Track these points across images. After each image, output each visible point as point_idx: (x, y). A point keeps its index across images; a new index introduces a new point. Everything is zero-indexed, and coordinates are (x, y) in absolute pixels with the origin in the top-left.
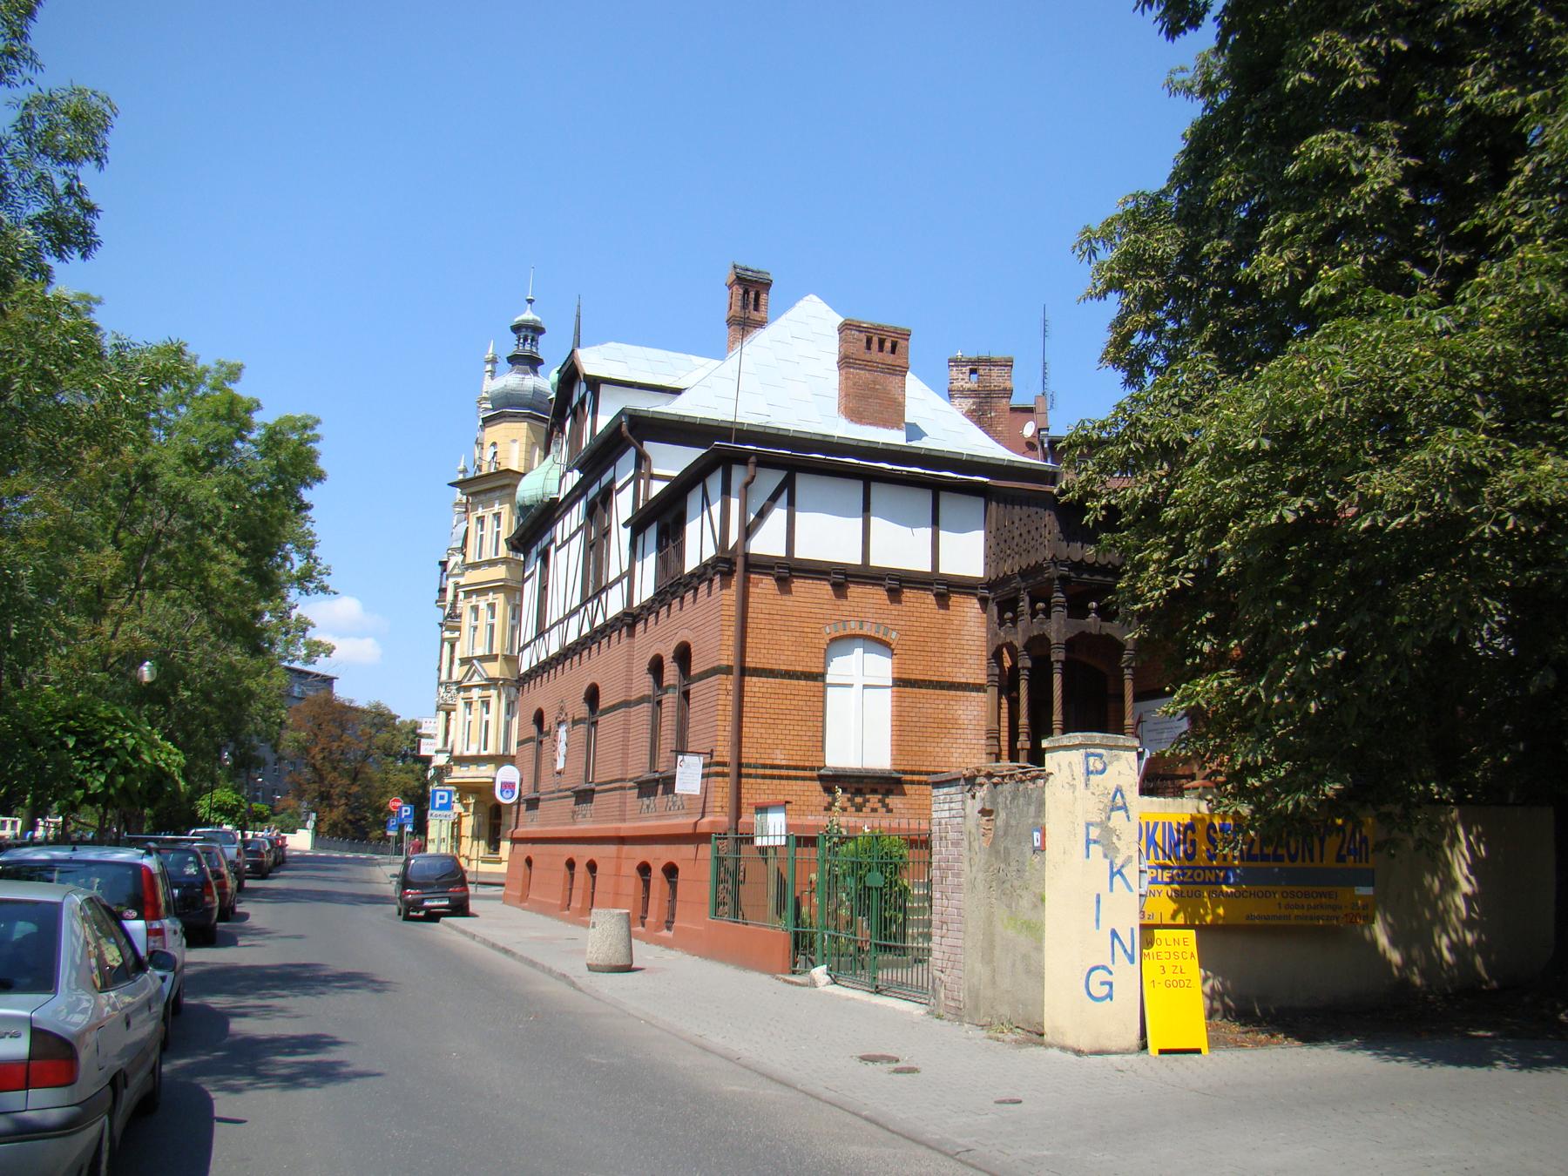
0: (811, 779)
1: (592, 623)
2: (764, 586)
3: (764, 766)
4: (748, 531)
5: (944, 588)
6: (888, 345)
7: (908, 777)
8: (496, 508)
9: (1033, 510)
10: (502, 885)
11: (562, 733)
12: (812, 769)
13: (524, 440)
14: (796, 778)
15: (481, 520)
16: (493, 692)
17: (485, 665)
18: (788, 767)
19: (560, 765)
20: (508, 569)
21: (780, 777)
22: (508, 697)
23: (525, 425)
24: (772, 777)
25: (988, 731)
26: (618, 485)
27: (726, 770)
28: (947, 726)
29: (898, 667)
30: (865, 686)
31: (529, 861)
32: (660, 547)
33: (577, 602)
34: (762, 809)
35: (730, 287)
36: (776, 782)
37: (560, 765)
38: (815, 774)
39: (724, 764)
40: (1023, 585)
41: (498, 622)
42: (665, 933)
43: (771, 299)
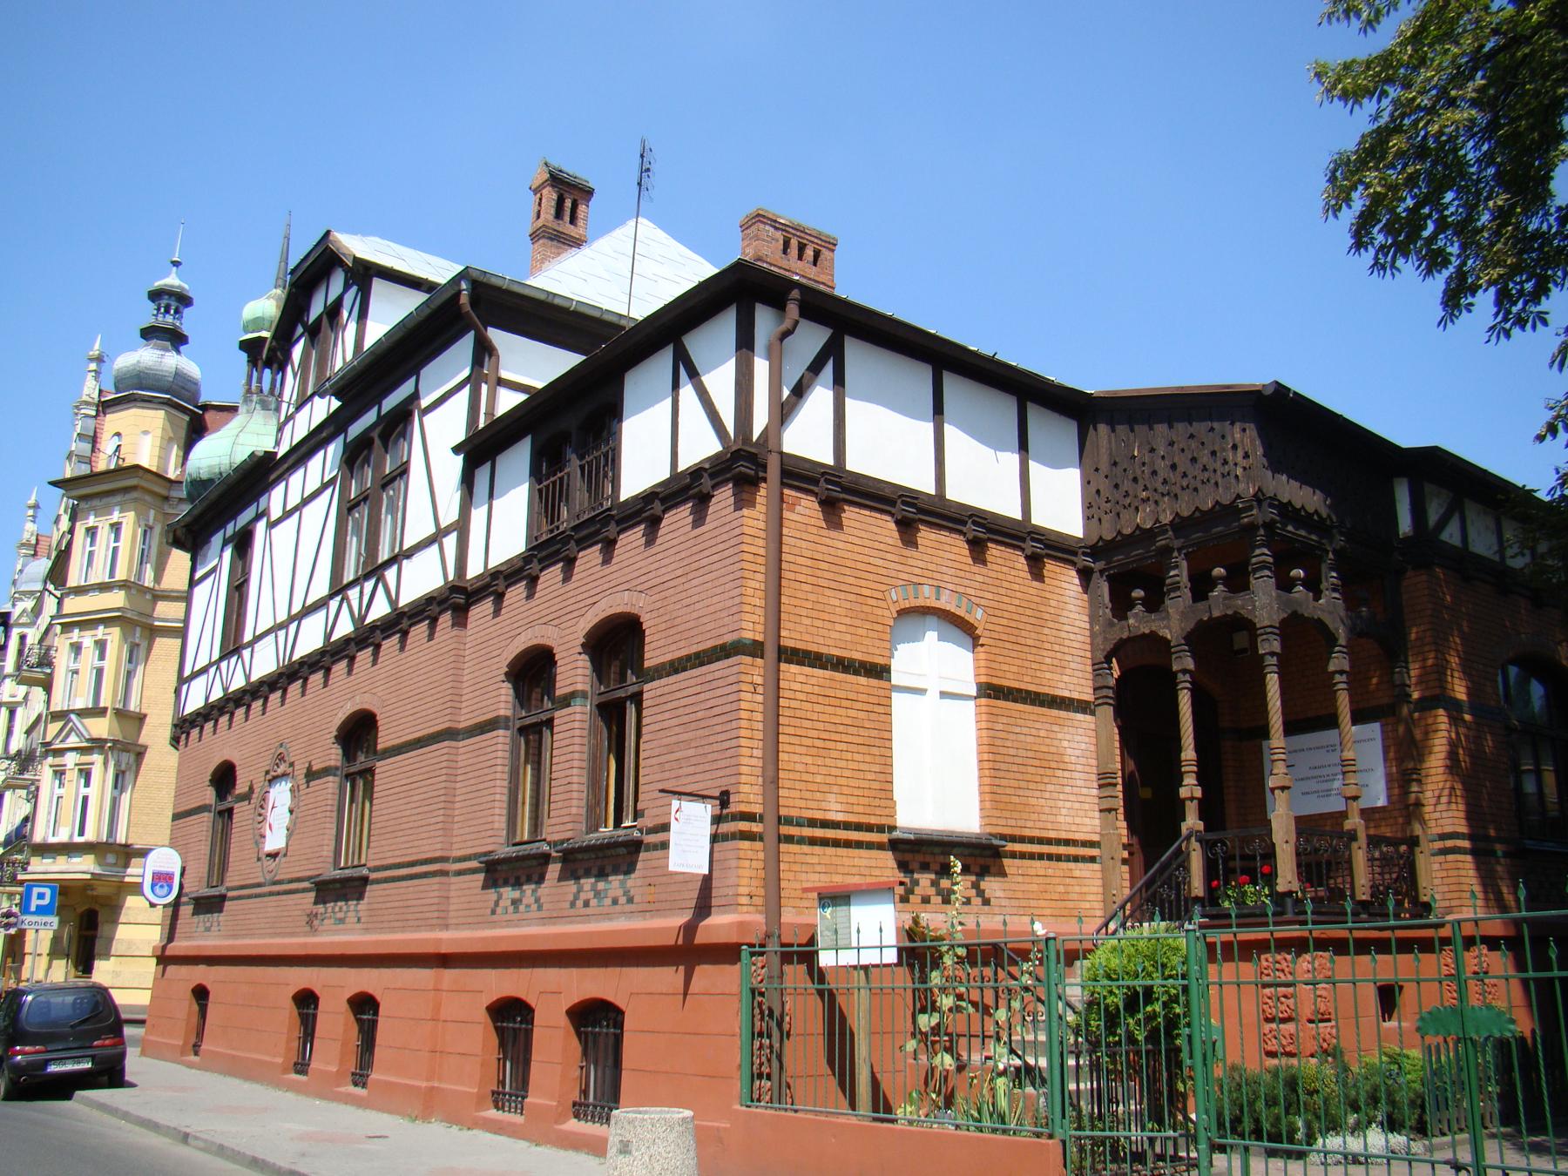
0: (880, 846)
1: (359, 620)
2: (804, 510)
3: (812, 823)
4: (783, 412)
6: (809, 253)
7: (1011, 847)
8: (116, 516)
9: (1200, 428)
10: (142, 1022)
11: (281, 795)
12: (880, 829)
13: (159, 432)
14: (859, 845)
15: (92, 532)
16: (97, 758)
17: (88, 721)
18: (847, 826)
19: (275, 840)
20: (128, 596)
21: (836, 843)
22: (118, 764)
23: (161, 414)
24: (824, 842)
25: (1102, 775)
26: (425, 403)
27: (756, 827)
28: (1049, 764)
30: (944, 695)
31: (201, 994)
32: (536, 474)
33: (321, 588)
34: (837, 897)
35: (537, 191)
36: (830, 850)
37: (275, 840)
38: (884, 838)
39: (750, 817)
40: (1177, 543)
41: (109, 665)
42: (193, 1058)
43: (591, 212)
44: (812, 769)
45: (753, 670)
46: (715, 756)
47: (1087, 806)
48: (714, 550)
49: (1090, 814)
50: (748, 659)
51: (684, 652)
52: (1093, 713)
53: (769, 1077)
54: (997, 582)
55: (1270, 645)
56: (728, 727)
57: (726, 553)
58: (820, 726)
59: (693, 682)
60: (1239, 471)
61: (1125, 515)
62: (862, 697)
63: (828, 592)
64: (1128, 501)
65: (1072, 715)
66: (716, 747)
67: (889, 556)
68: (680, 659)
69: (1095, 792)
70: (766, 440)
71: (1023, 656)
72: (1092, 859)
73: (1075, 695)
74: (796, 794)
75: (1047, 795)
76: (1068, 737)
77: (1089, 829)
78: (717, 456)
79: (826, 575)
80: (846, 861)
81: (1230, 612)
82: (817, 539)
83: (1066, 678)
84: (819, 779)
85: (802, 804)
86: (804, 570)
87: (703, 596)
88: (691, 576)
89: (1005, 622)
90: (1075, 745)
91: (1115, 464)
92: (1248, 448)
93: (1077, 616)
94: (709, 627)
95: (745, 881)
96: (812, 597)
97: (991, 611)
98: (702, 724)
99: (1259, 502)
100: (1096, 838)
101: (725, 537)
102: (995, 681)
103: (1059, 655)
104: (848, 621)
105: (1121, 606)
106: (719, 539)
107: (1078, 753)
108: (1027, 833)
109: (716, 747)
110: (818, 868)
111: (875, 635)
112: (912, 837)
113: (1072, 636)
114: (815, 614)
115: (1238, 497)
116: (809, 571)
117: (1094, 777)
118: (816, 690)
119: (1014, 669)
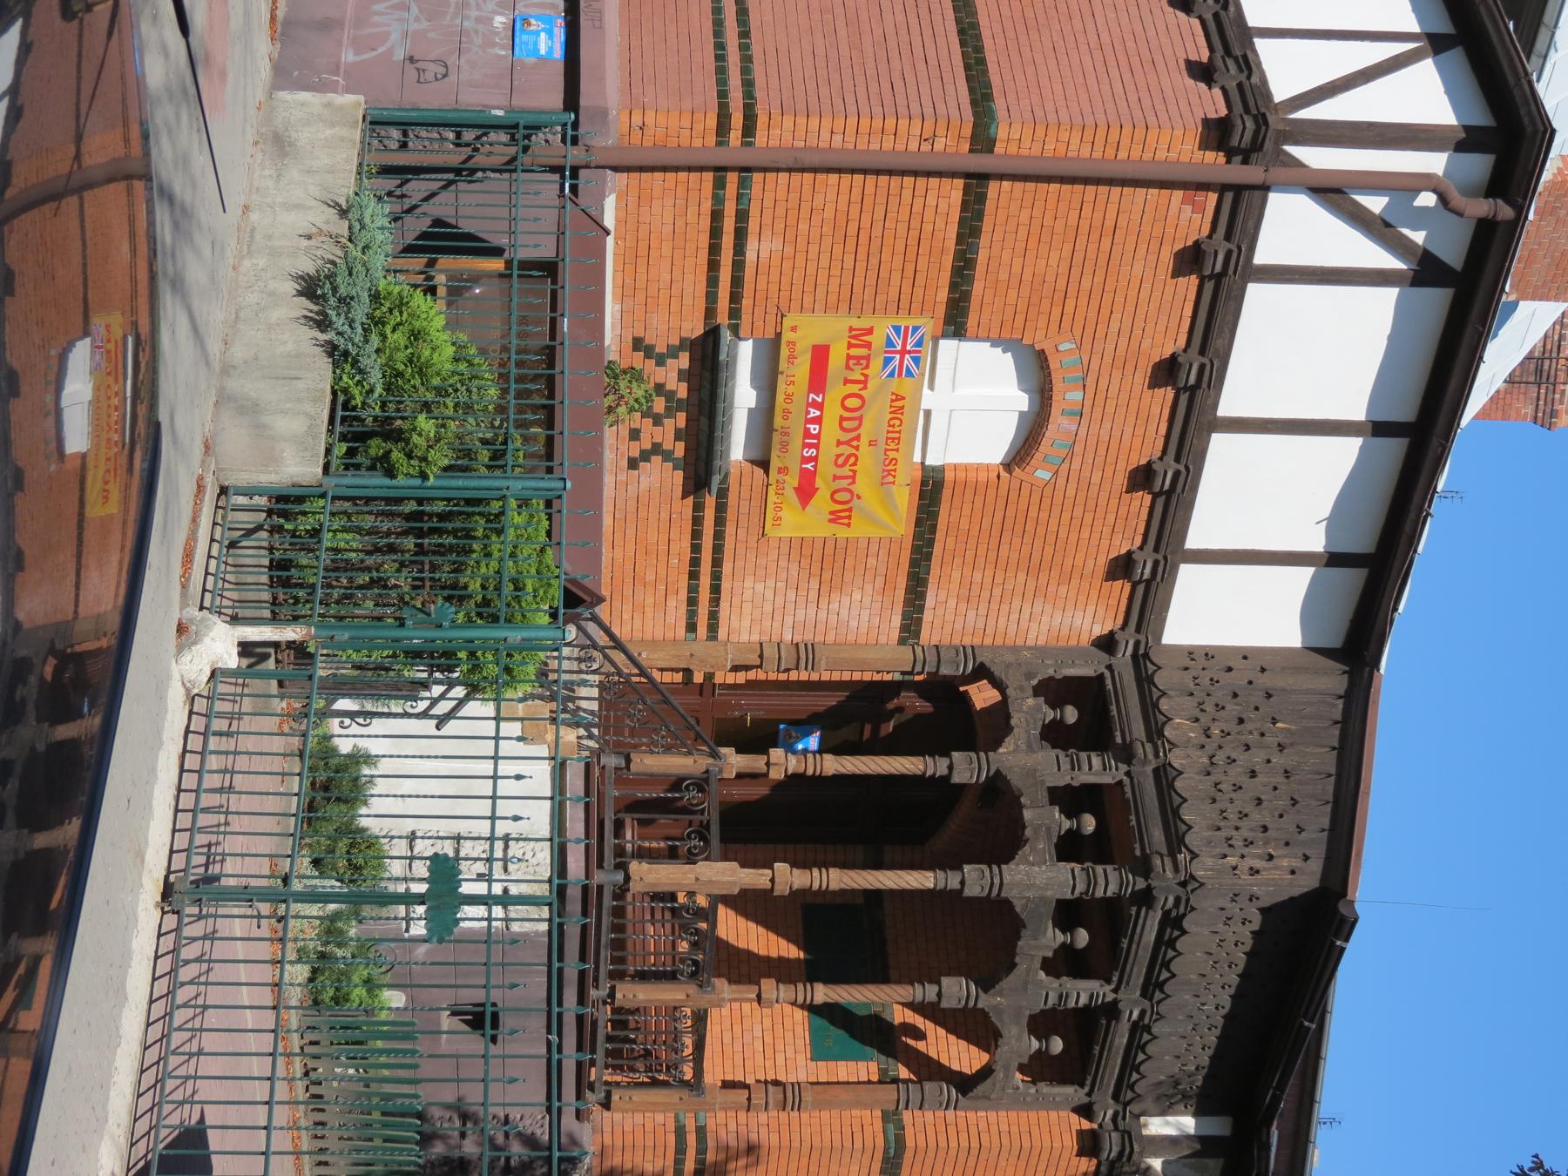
0: (710, 312)
2: (1190, 219)
4: (1332, 192)
5: (1145, 576)
7: (710, 501)
12: (735, 313)
14: (712, 282)
18: (739, 265)
21: (714, 249)
24: (716, 233)
25: (811, 648)
27: (735, 136)
28: (826, 564)
29: (972, 480)
38: (722, 318)
39: (749, 129)
44: (816, 220)
45: (952, 144)
46: (836, 83)
47: (767, 623)
48: (1130, 88)
49: (756, 629)
50: (967, 131)
51: (988, 43)
52: (902, 641)
53: (404, 145)
54: (1091, 504)
55: (974, 880)
56: (875, 101)
57: (1122, 104)
58: (877, 232)
59: (944, 53)
60: (1231, 860)
61: (1190, 703)
62: (919, 292)
63: (1068, 247)
64: (1209, 707)
65: (899, 609)
66: (848, 85)
67: (1123, 341)
68: (978, 37)
69: (788, 637)
70: (1285, 165)
71: (984, 539)
72: (691, 627)
73: (927, 616)
74: (781, 195)
75: (783, 563)
76: (867, 600)
77: (735, 623)
78: (1267, 95)
79: (1093, 247)
80: (690, 262)
81: (1028, 832)
82: (1144, 237)
83: (952, 602)
84: (803, 226)
85: (768, 203)
86: (1098, 215)
87: (1066, 72)
88: (1097, 54)
89: (1033, 513)
90: (855, 612)
91: (1269, 696)
92: (1264, 875)
93: (1044, 628)
94: (1020, 78)
95: (662, 119)
96: (1060, 224)
97: (1048, 492)
98: (883, 67)
99: (1183, 884)
100: (722, 633)
101: (1147, 103)
102: (946, 493)
103: (986, 594)
104: (1027, 277)
105: (1055, 690)
106: (1144, 95)
107: (844, 613)
108: (730, 530)
109: (848, 85)
110: (680, 223)
111: (1008, 316)
112: (722, 357)
113: (1014, 617)
114: (1035, 228)
115: (1194, 856)
116: (1097, 223)
117: (809, 637)
118: (928, 228)
119: (964, 525)
